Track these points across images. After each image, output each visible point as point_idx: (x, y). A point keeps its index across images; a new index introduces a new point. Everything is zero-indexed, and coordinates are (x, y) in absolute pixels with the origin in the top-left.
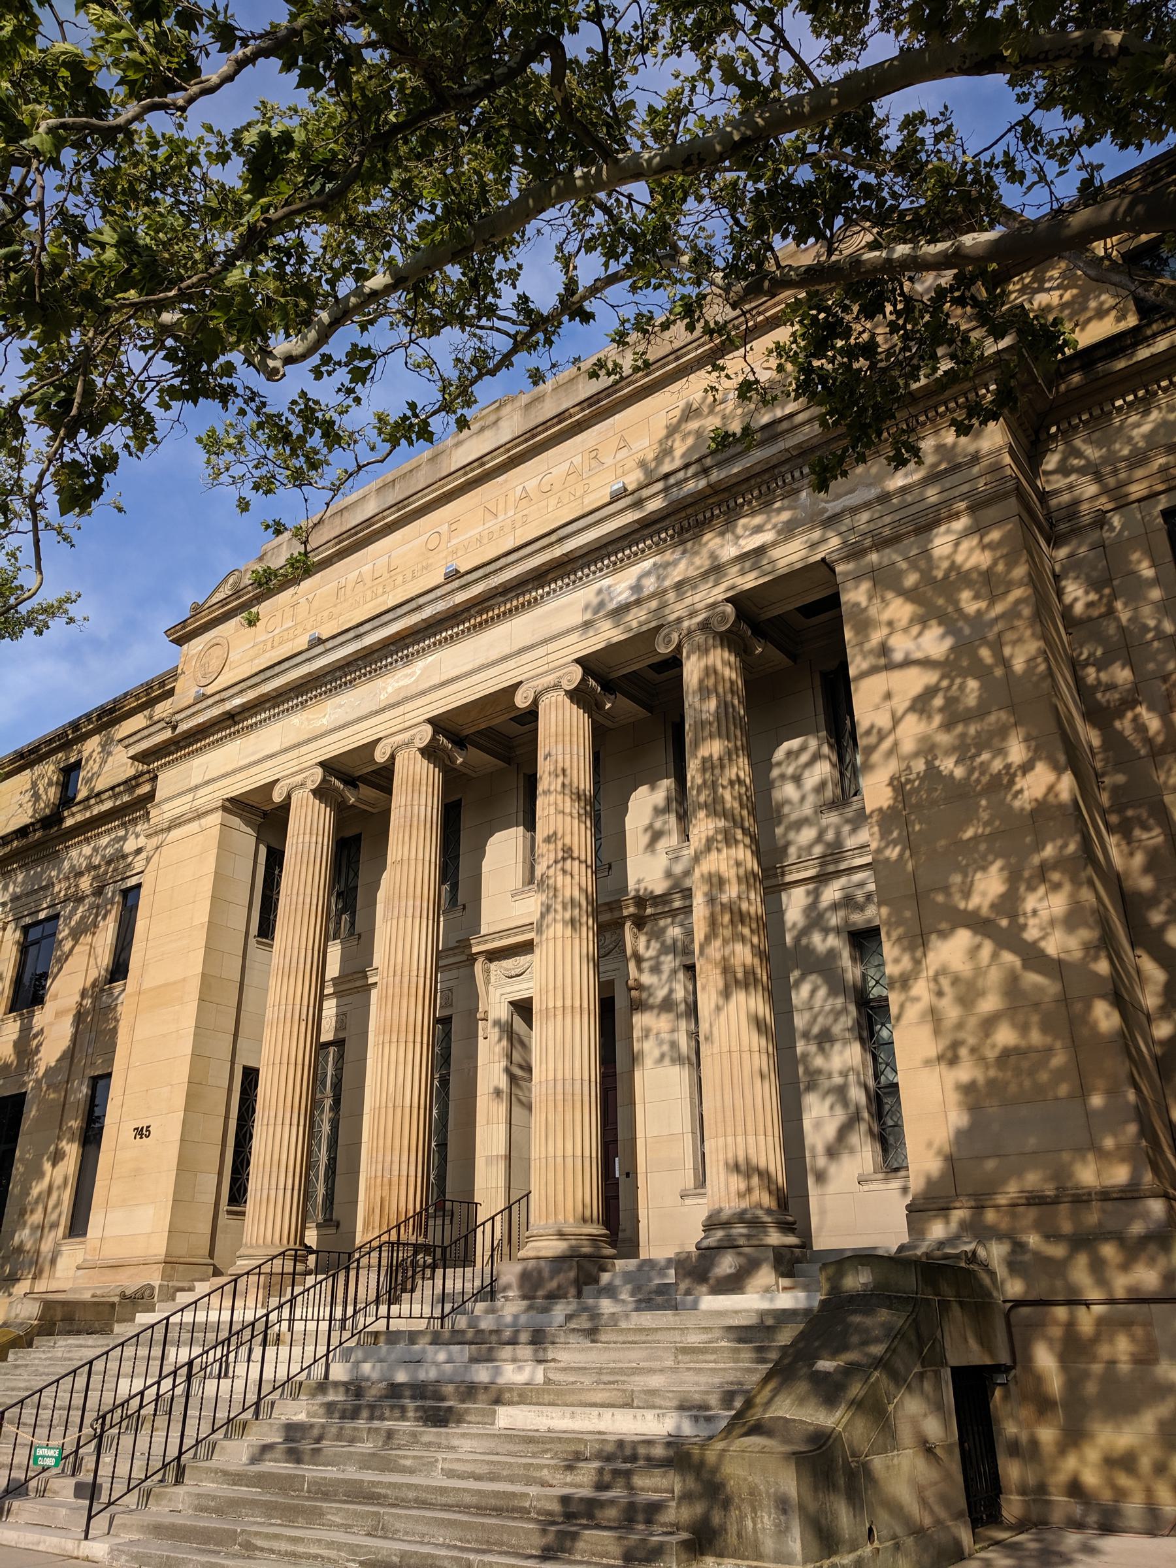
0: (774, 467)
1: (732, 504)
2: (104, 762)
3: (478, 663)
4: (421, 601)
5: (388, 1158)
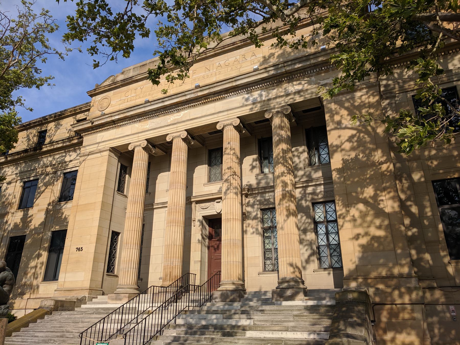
0: (305, 68)
1: (291, 77)
2: (56, 131)
3: (204, 114)
4: (186, 93)
5: (172, 260)
